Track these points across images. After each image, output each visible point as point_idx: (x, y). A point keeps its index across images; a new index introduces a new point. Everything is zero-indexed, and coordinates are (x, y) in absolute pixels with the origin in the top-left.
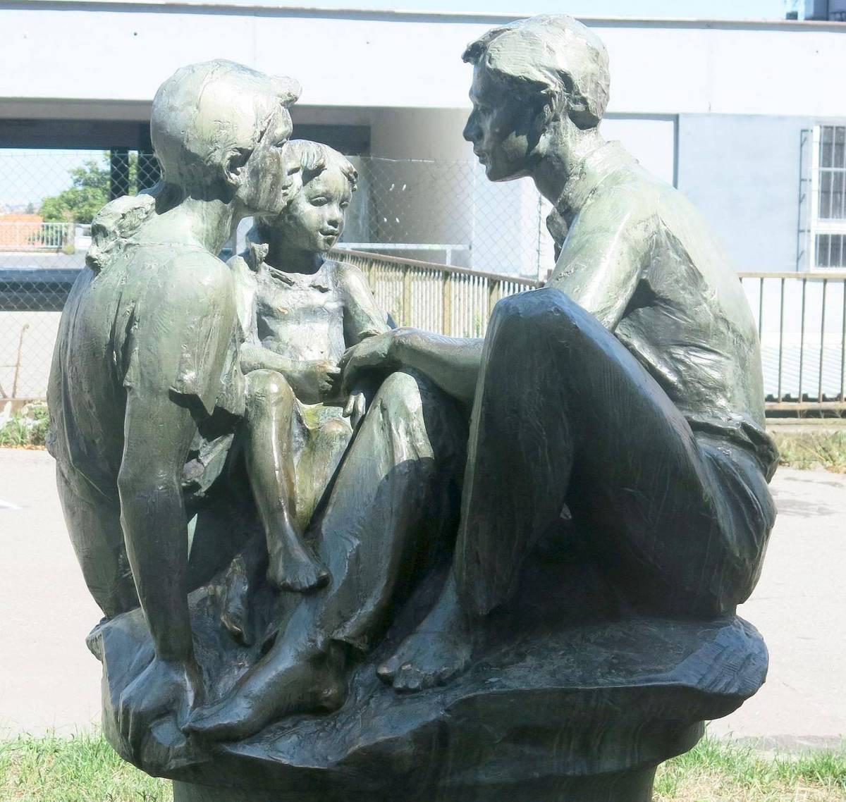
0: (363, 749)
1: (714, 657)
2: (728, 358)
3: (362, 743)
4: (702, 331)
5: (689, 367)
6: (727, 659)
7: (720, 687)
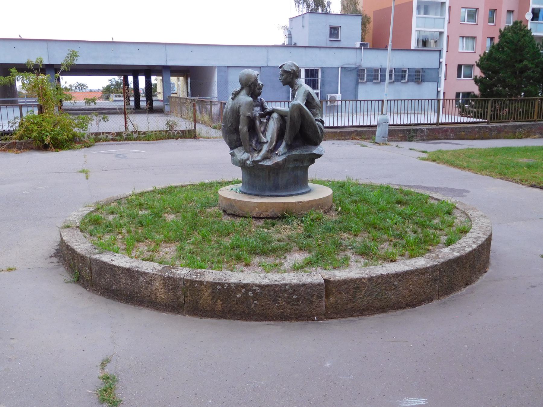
3: (275, 162)
7: (319, 154)
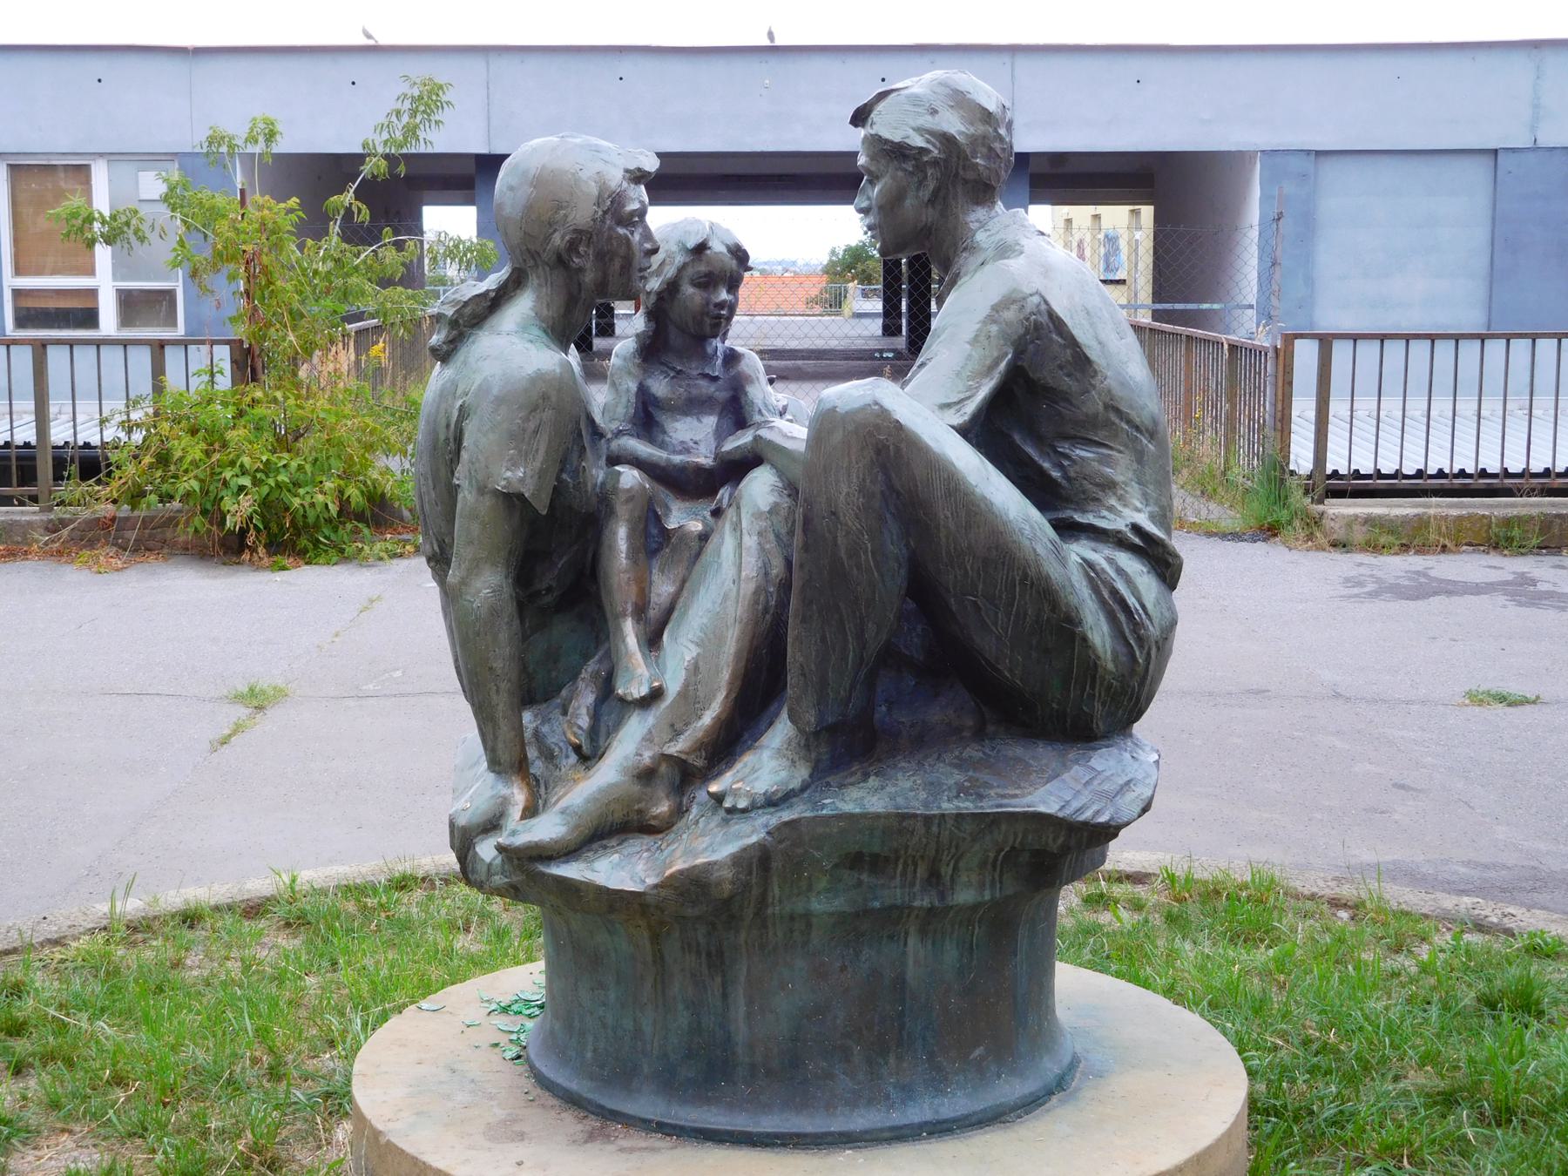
0: (681, 872)
1: (1084, 782)
2: (1120, 452)
3: (679, 865)
4: (1093, 422)
5: (1074, 461)
6: (1100, 784)
7: (1086, 816)
